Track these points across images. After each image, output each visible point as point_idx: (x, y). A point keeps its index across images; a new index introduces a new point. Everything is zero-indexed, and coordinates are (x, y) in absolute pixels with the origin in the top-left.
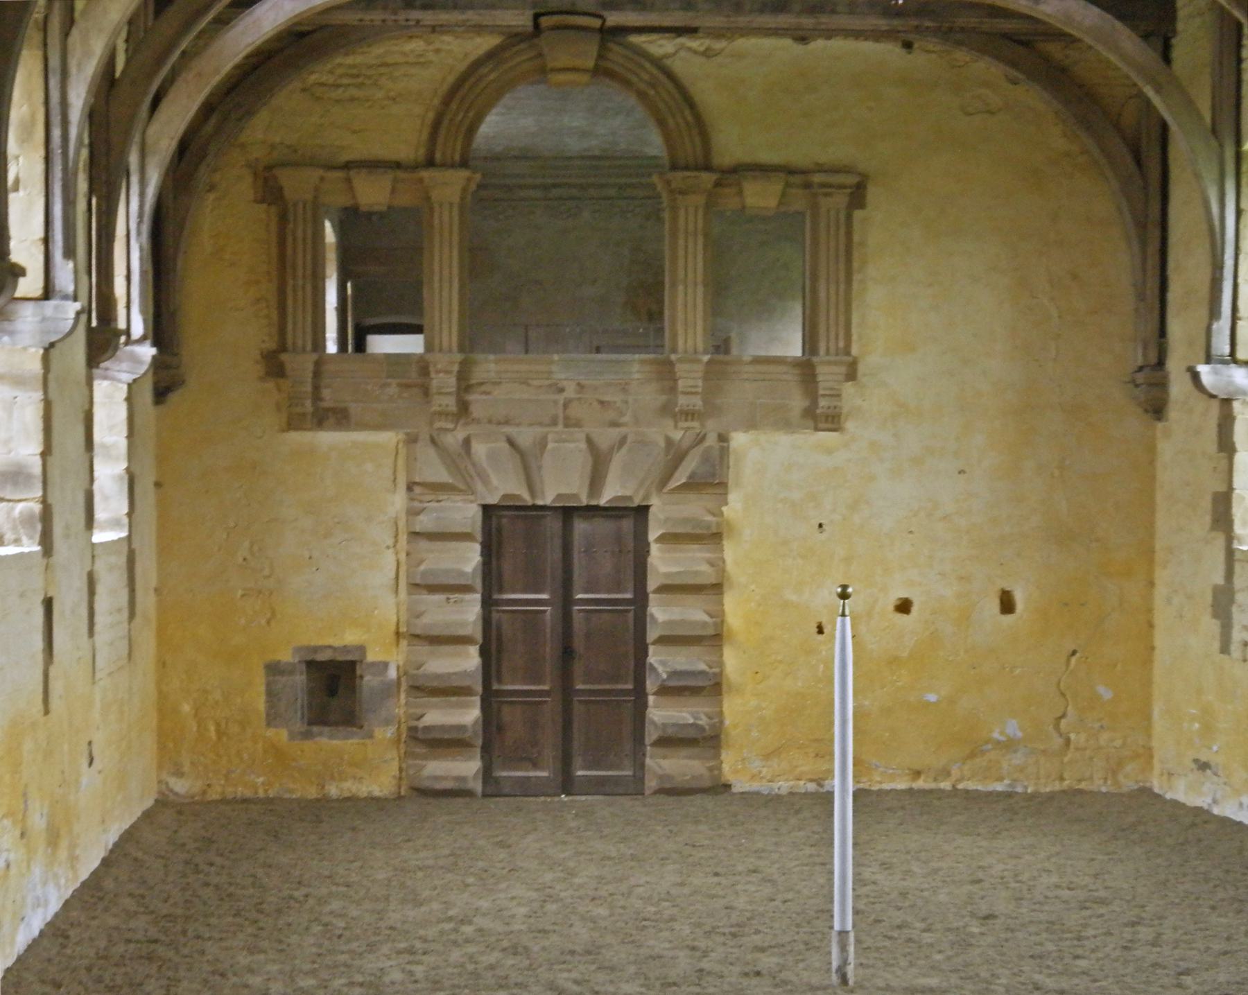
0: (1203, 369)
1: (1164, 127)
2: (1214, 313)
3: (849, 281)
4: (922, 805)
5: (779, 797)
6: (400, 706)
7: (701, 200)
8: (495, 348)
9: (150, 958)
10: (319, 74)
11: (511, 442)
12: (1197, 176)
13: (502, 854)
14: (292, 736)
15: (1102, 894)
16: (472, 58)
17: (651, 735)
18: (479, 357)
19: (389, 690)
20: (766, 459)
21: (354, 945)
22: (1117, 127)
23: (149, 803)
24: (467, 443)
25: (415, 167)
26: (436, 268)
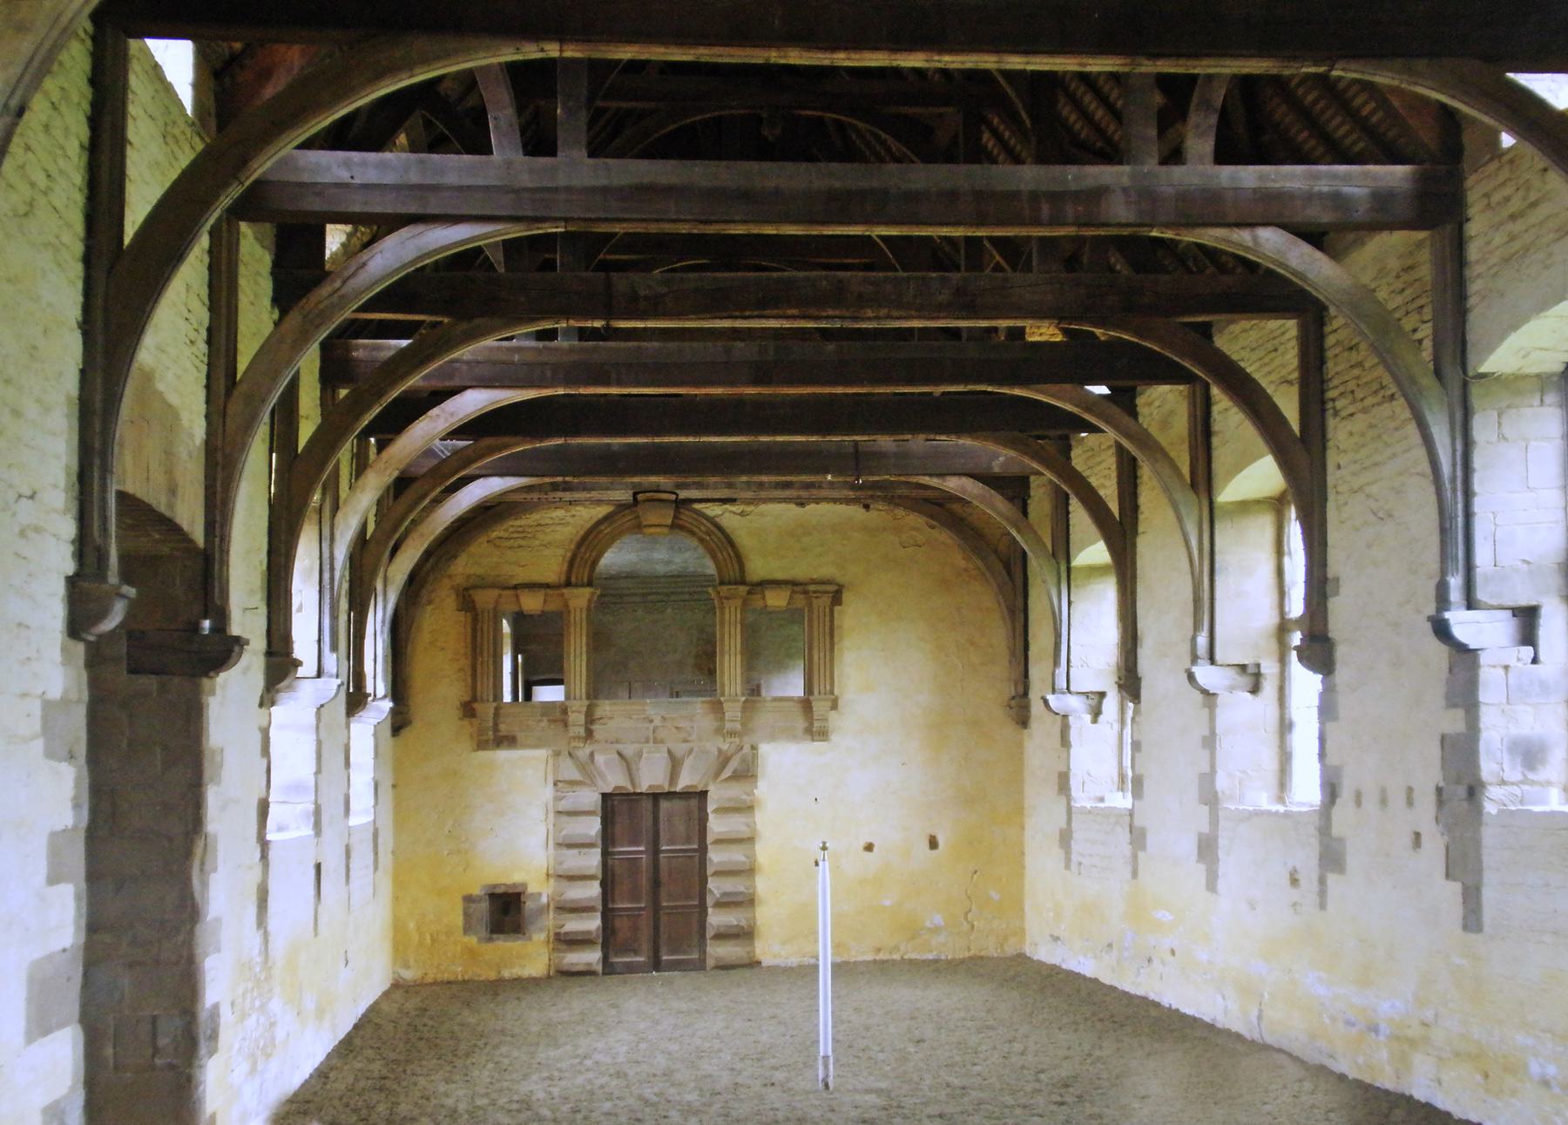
0: (1050, 697)
1: (1024, 554)
2: (1056, 663)
3: (832, 649)
4: (882, 969)
5: (792, 968)
6: (550, 920)
7: (739, 602)
8: (611, 695)
9: (381, 1090)
10: (497, 532)
11: (620, 754)
13: (614, 1012)
14: (480, 940)
15: (991, 1022)
17: (710, 933)
18: (600, 702)
19: (543, 910)
20: (783, 763)
21: (515, 1076)
22: (996, 552)
23: (386, 986)
24: (592, 754)
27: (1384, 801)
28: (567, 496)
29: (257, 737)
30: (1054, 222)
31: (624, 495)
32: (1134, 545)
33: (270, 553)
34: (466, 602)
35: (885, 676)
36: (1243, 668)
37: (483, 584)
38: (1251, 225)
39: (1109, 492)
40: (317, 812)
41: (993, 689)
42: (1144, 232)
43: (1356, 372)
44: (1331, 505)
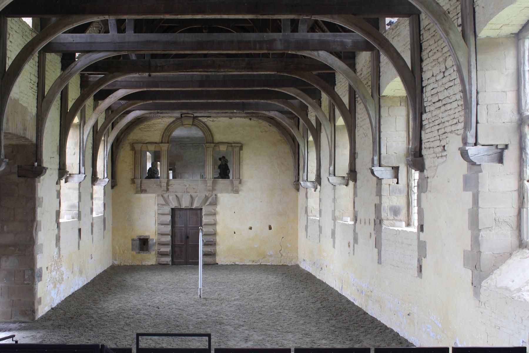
6: (156, 248)
7: (212, 149)
10: (142, 126)
11: (176, 196)
14: (136, 253)
20: (226, 201)
24: (168, 196)
25: (159, 143)
28: (162, 115)
29: (55, 194)
30: (261, 49)
32: (320, 136)
33: (60, 140)
35: (257, 173)
37: (137, 142)
38: (317, 50)
40: (79, 213)
41: (290, 178)
42: (286, 52)
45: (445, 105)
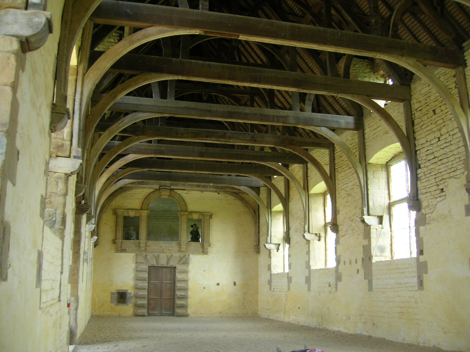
0: (266, 245)
2: (268, 236)
6: (133, 300)
10: (124, 194)
12: (265, 215)
14: (115, 305)
16: (149, 193)
19: (131, 297)
24: (146, 255)
25: (139, 210)
26: (142, 226)
27: (350, 263)
28: (143, 186)
31: (157, 187)
32: (288, 204)
34: (115, 212)
36: (316, 234)
39: (282, 190)
43: (342, 162)
44: (337, 193)
45: (441, 160)
